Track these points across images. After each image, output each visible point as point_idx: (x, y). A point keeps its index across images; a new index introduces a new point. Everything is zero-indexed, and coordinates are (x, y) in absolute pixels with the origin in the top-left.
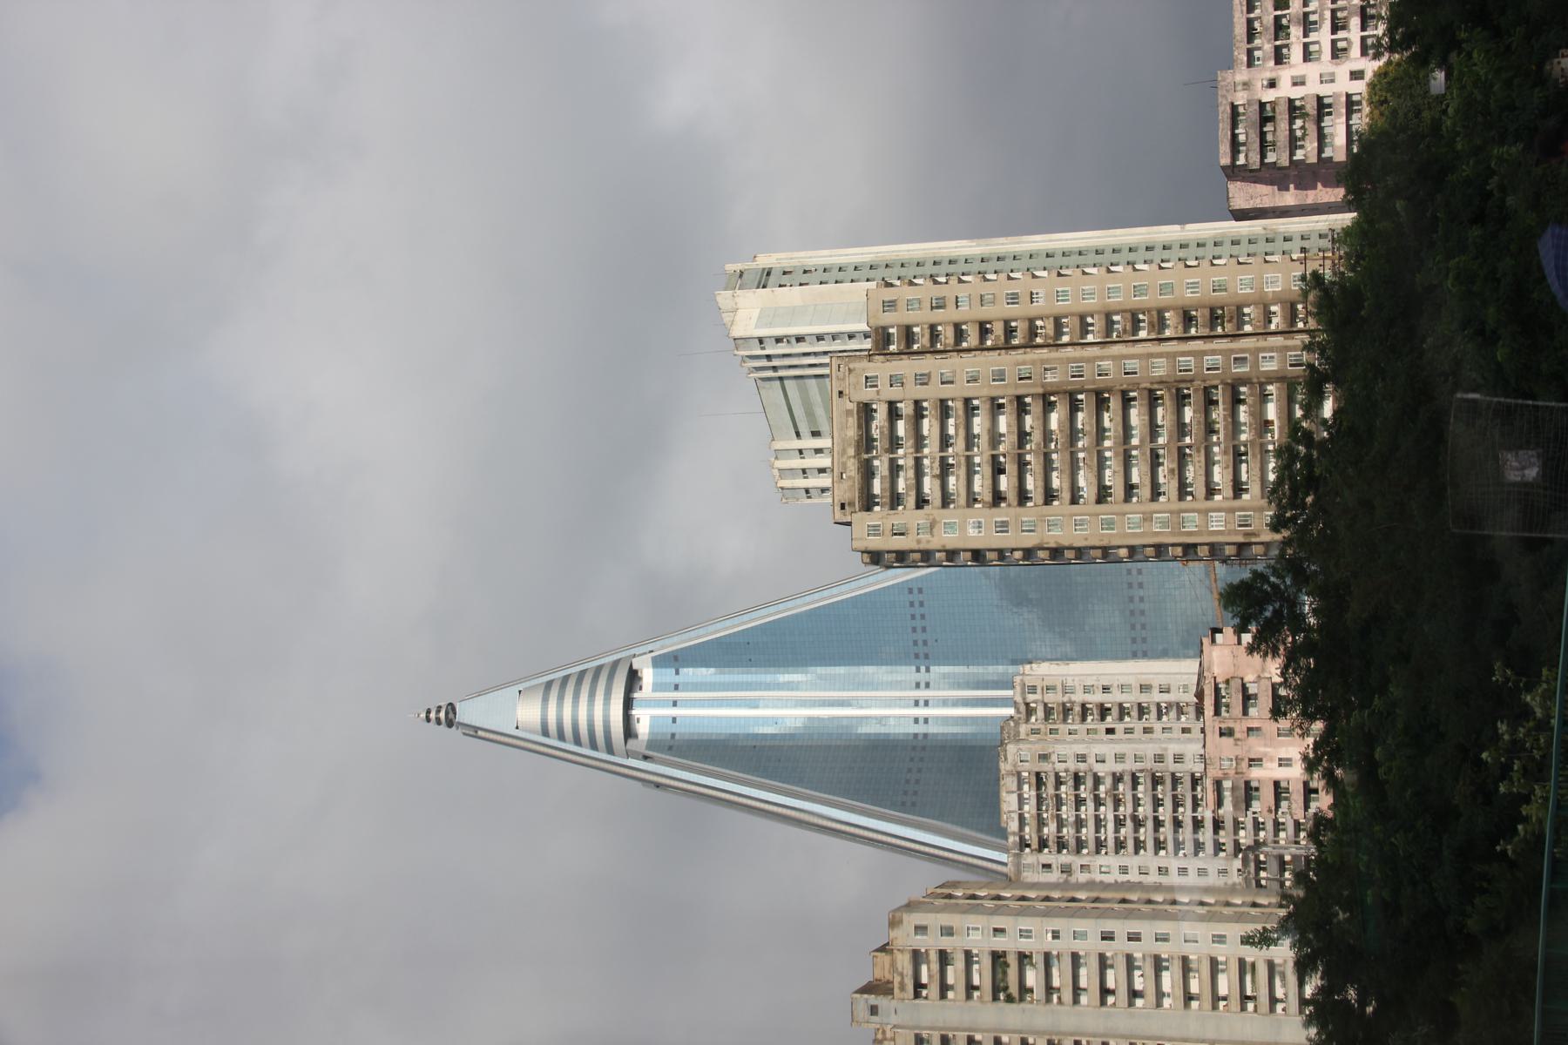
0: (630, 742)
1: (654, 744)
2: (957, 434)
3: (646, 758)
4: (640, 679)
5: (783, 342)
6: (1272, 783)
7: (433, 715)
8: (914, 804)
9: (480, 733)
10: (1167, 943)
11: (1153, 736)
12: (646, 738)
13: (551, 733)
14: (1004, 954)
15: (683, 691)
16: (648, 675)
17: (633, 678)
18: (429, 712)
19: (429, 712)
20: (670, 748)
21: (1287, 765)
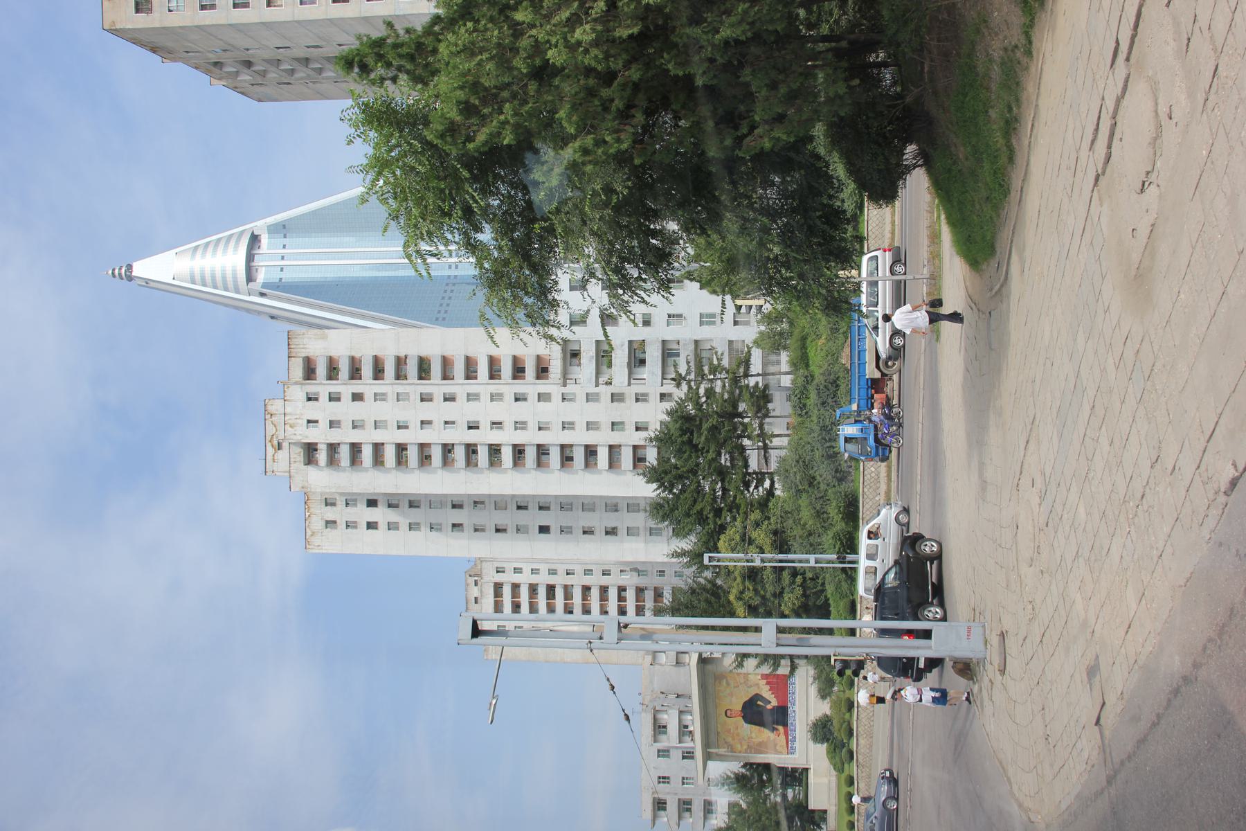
0: (250, 284)
1: (265, 285)
2: (733, 465)
3: (263, 295)
4: (260, 241)
5: (927, 660)
6: (370, 508)
7: (117, 272)
8: (444, 319)
9: (152, 284)
10: (622, 404)
11: (845, 814)
12: (262, 281)
13: (229, 286)
14: (429, 445)
15: (289, 249)
16: (265, 240)
17: (255, 239)
18: (114, 270)
19: (114, 270)
20: (278, 286)
21: (522, 429)
